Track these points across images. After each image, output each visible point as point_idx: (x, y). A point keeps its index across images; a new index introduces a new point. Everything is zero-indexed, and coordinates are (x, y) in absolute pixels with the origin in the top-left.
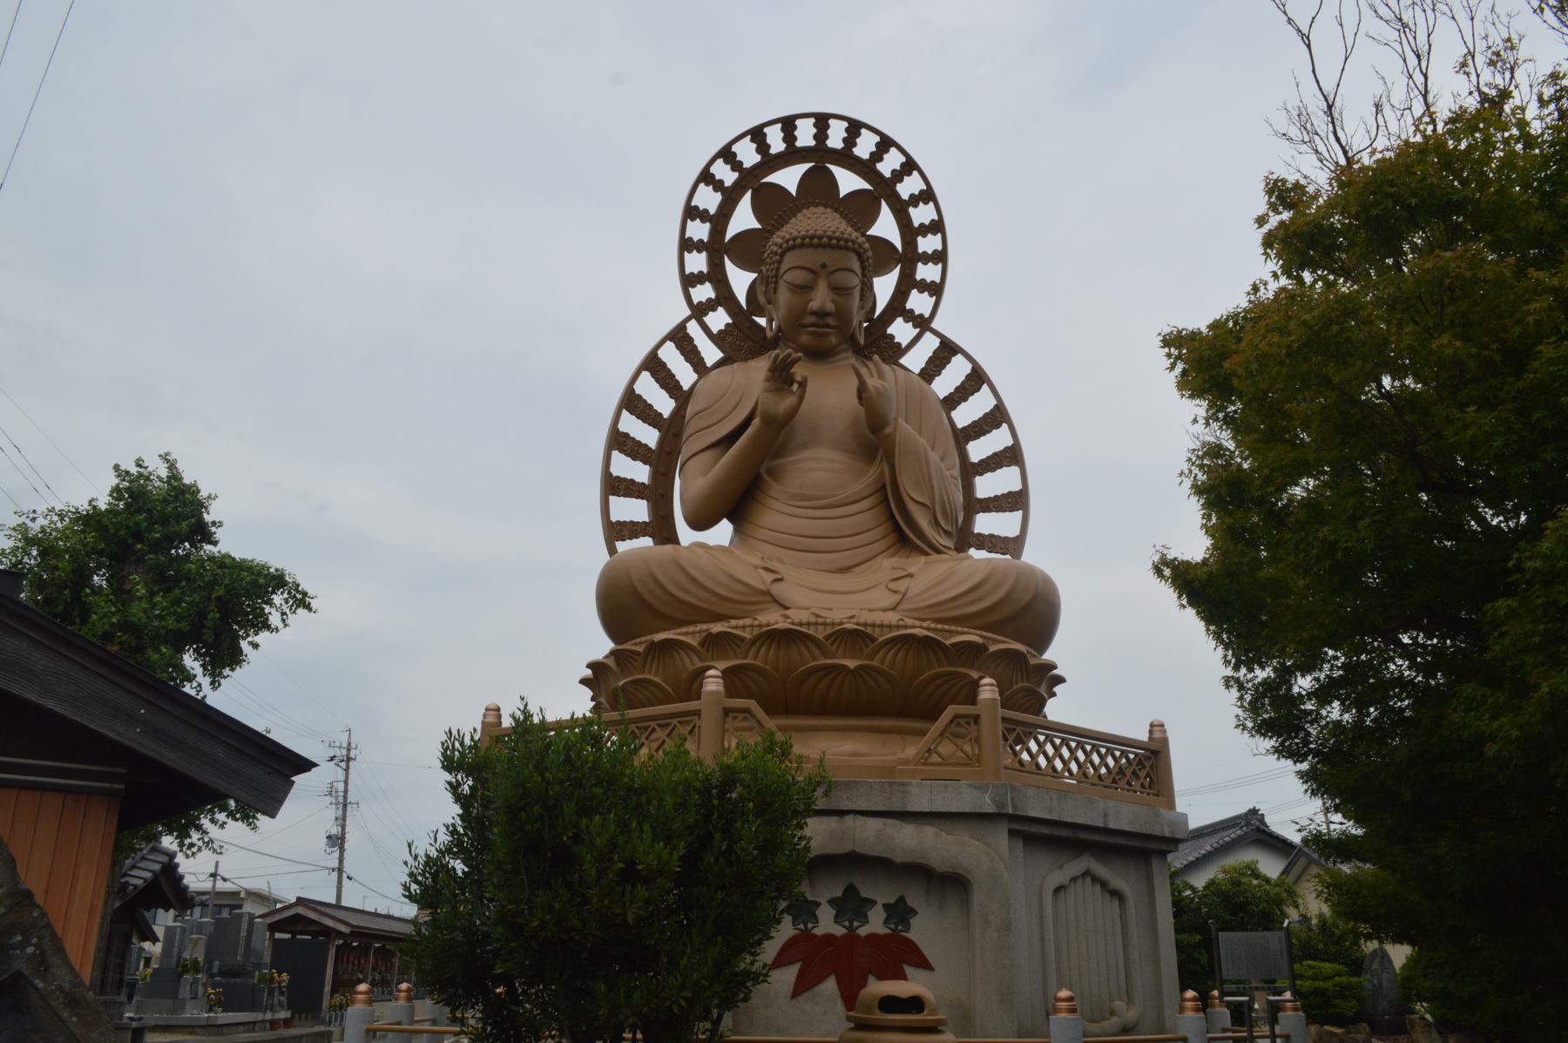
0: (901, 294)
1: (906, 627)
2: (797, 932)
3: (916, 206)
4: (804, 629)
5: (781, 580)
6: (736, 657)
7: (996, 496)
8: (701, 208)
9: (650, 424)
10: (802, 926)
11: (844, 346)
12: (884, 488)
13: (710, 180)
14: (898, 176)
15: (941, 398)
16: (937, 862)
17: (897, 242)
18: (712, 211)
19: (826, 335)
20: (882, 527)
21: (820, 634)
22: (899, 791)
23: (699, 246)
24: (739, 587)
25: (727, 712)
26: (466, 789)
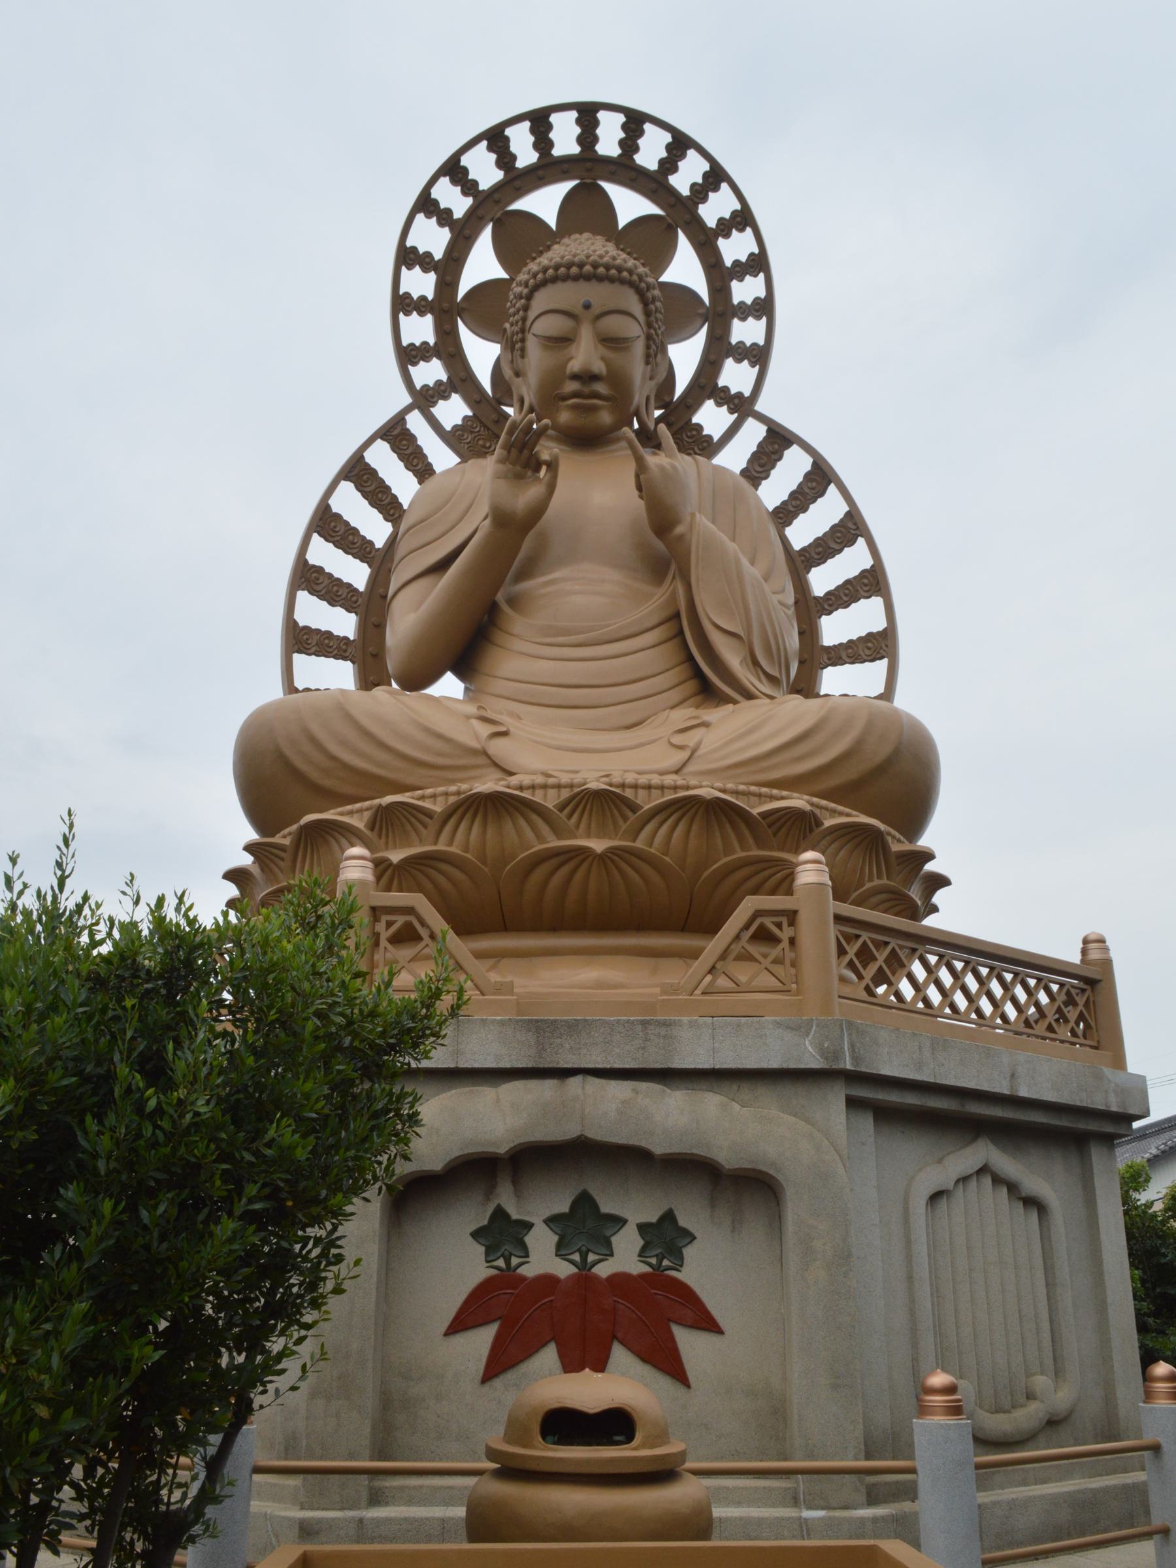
0: (709, 366)
1: (688, 788)
2: (494, 1272)
3: (727, 235)
4: (526, 795)
5: (505, 734)
7: (851, 641)
8: (421, 251)
9: (355, 556)
10: (501, 1263)
12: (677, 616)
14: (701, 192)
16: (725, 1156)
17: (703, 291)
18: (438, 255)
19: (594, 409)
21: (550, 801)
22: (659, 1035)
23: (420, 306)
24: (439, 745)
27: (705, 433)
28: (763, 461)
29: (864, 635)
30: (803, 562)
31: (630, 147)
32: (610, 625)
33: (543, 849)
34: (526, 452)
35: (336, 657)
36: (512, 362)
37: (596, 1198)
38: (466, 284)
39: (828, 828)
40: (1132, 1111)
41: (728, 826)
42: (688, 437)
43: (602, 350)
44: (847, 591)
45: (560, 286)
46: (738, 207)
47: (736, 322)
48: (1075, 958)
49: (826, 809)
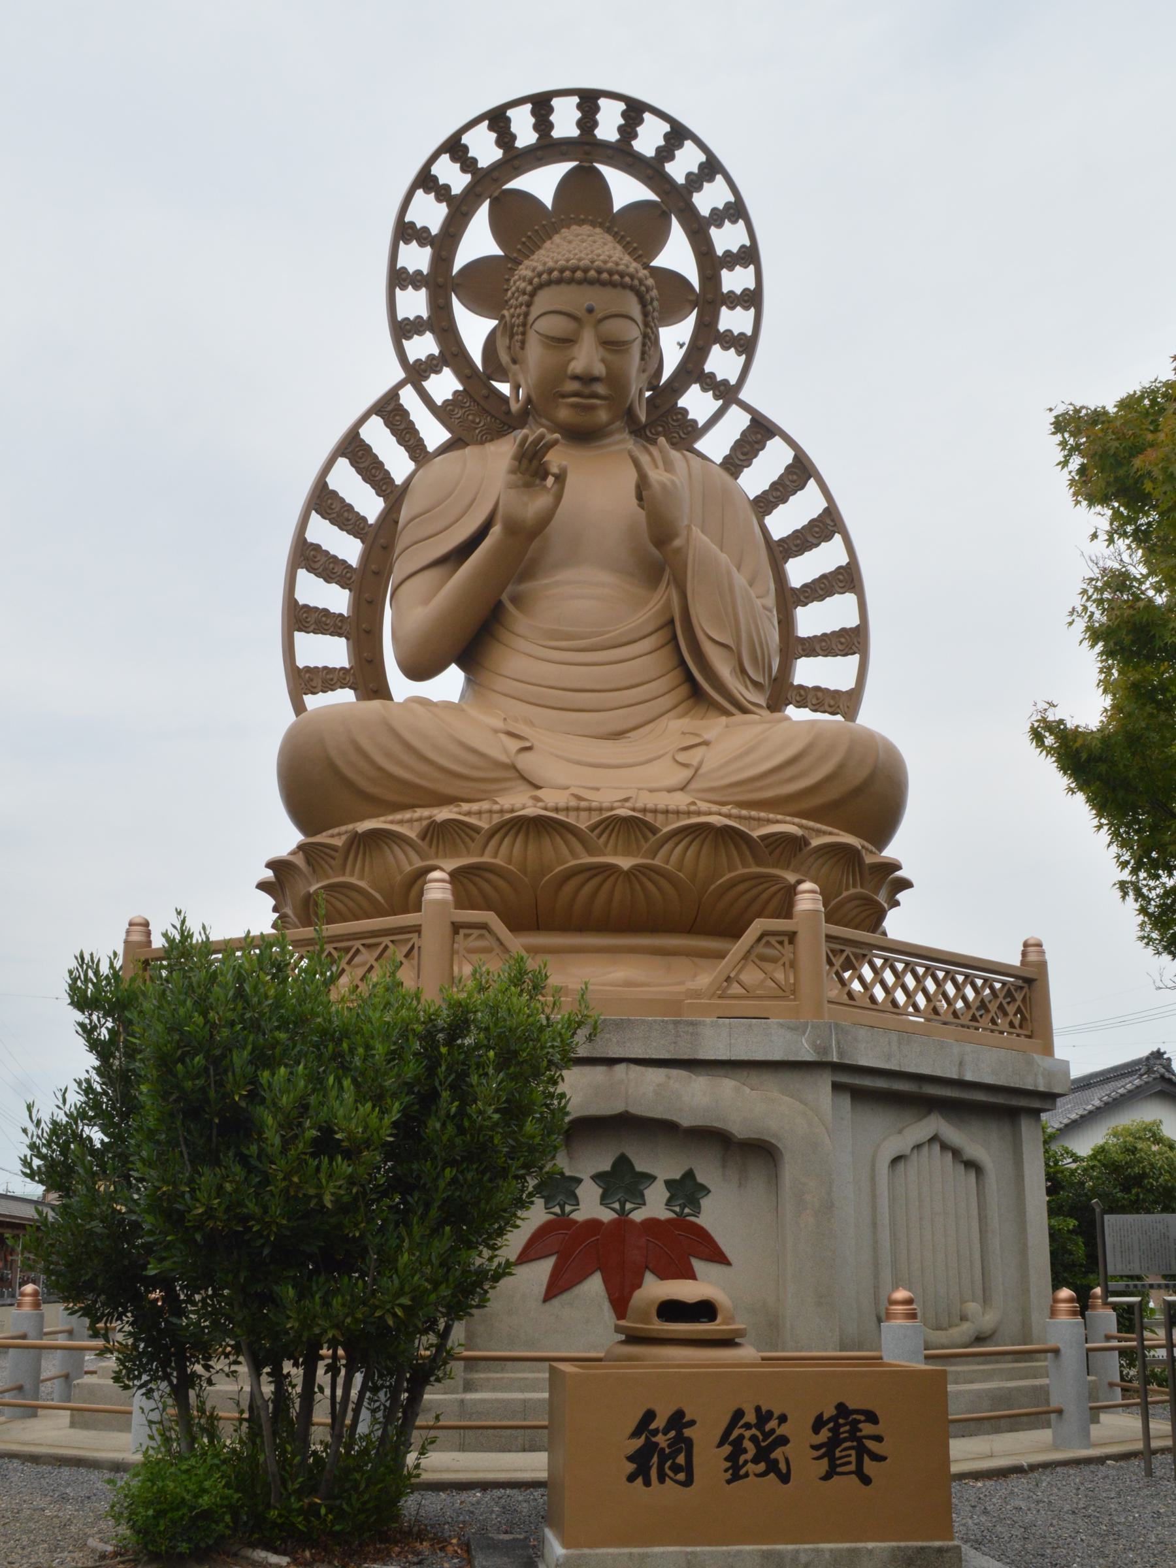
0: (697, 352)
1: (699, 813)
2: (551, 1217)
3: (720, 225)
4: (560, 816)
6: (469, 853)
7: (824, 635)
8: (419, 226)
9: (349, 532)
10: (557, 1210)
11: (618, 424)
12: (671, 622)
13: (431, 184)
14: (696, 181)
15: (751, 498)
16: (738, 1129)
17: (694, 278)
18: (435, 230)
19: (592, 408)
20: (669, 675)
24: (473, 759)
25: (456, 927)
26: (104, 1034)
27: (690, 417)
28: (745, 450)
29: (837, 629)
30: (781, 552)
31: (630, 133)
32: (609, 632)
33: (577, 865)
34: (535, 463)
35: (332, 634)
36: (509, 348)
37: (633, 1160)
38: (461, 259)
39: (815, 847)
40: (1056, 1091)
41: (733, 849)
42: (673, 420)
43: (602, 352)
44: (822, 586)
45: (563, 288)
46: (732, 199)
47: (724, 310)
48: (1015, 960)
49: (812, 829)
